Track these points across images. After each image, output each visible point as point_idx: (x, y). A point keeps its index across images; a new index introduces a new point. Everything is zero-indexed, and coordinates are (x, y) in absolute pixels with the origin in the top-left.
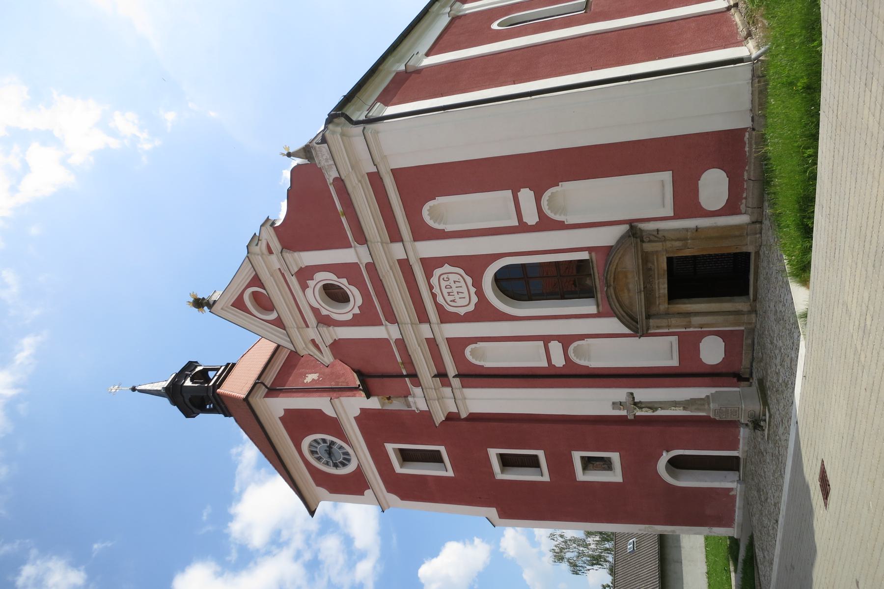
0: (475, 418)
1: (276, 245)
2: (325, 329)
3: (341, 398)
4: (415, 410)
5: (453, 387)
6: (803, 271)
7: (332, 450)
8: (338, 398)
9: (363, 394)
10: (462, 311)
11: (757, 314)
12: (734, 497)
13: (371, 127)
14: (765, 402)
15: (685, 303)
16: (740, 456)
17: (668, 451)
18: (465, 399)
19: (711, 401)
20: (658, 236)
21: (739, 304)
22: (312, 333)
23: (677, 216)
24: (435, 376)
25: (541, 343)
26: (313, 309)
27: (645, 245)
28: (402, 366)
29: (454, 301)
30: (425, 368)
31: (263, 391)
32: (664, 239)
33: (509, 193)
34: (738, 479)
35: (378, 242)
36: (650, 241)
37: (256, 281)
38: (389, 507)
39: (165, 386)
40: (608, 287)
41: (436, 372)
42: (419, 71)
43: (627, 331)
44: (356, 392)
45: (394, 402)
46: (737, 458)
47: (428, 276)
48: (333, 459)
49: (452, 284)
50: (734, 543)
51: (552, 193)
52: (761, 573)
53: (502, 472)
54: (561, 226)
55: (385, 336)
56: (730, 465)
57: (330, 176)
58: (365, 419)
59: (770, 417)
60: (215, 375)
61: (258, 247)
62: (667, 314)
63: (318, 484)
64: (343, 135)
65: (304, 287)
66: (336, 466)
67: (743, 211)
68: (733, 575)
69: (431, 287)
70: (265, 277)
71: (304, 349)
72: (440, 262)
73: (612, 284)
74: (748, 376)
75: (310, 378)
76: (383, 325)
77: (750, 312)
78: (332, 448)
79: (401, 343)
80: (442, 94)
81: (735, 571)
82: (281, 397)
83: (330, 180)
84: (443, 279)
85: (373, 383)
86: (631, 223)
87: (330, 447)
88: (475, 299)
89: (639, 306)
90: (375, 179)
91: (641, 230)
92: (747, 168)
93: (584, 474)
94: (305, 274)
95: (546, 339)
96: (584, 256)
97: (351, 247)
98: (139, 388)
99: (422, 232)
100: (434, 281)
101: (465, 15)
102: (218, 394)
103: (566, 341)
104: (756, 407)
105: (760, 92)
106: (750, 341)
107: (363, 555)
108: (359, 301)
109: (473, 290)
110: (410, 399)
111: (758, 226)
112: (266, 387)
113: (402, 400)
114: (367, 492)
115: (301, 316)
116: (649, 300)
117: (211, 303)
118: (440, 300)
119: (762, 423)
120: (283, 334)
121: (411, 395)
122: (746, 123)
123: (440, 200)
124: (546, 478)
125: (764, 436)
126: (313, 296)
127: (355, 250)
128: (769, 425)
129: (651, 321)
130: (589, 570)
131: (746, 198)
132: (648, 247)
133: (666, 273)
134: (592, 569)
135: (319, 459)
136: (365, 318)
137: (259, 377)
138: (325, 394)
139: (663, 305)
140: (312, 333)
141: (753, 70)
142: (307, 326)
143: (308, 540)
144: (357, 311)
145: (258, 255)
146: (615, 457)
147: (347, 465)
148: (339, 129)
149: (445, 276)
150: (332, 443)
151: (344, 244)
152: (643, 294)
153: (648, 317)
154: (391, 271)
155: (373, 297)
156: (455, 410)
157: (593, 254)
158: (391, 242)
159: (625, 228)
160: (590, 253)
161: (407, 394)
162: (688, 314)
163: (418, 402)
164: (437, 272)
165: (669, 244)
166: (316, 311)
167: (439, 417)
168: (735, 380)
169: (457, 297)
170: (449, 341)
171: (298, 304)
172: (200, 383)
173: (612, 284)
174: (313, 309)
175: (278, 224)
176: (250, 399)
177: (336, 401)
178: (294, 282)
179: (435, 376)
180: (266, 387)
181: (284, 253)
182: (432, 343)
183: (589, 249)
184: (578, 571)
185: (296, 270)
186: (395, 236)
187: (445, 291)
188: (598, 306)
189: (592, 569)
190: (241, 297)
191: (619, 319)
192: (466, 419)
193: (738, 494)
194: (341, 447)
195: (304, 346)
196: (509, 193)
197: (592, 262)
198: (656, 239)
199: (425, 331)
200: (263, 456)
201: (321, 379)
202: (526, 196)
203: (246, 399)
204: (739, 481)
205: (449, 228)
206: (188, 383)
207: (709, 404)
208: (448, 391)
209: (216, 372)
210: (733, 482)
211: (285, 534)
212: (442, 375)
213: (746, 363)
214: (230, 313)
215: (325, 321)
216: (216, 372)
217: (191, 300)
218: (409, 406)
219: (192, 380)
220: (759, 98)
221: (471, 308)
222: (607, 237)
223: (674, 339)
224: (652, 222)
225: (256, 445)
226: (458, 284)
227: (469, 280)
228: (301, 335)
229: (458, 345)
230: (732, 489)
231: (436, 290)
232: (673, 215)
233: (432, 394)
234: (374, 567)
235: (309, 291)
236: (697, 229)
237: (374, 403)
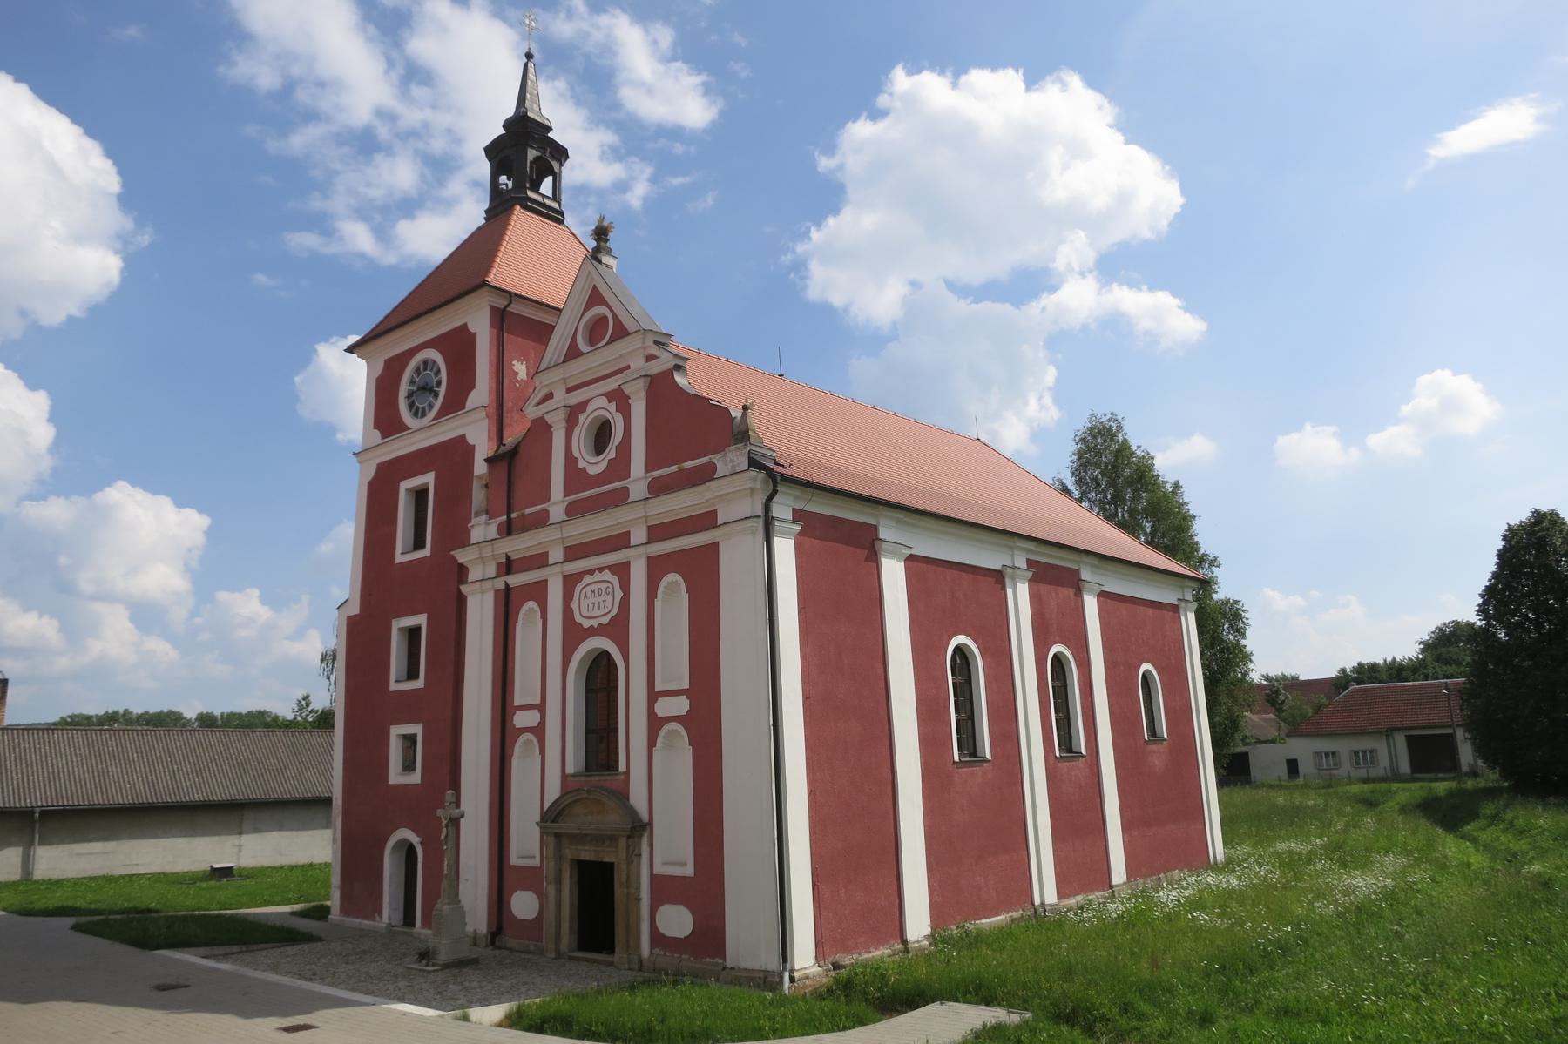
0: (461, 601)
1: (655, 368)
2: (563, 416)
3: (487, 420)
4: (471, 522)
5: (495, 580)
6: (515, 1021)
7: (427, 393)
8: (487, 416)
9: (491, 454)
10: (574, 605)
11: (555, 959)
12: (373, 919)
13: (760, 524)
14: (446, 966)
15: (571, 878)
16: (415, 930)
17: (421, 843)
18: (482, 593)
19: (451, 906)
20: (633, 855)
21: (567, 939)
22: (560, 397)
23: (654, 879)
24: (508, 557)
25: (539, 702)
26: (586, 402)
27: (625, 839)
28: (520, 513)
29: (586, 596)
30: (518, 545)
31: (501, 303)
32: (629, 862)
33: (686, 685)
34: (393, 924)
35: (646, 512)
36: (628, 846)
37: (621, 332)
38: (360, 463)
39: (529, 114)
40: (588, 791)
41: (513, 558)
42: (873, 557)
43: (546, 806)
44: (495, 440)
45: (483, 492)
46: (413, 925)
47: (614, 569)
48: (418, 393)
49: (602, 598)
50: (321, 913)
51: (683, 736)
52: (271, 951)
53: (401, 629)
54: (652, 742)
55: (553, 498)
56: (409, 919)
57: (718, 460)
58: (459, 450)
59: (429, 972)
60: (543, 196)
61: (652, 344)
62: (559, 857)
63: (389, 363)
64: (752, 490)
65: (610, 396)
66: (410, 395)
67: (654, 951)
68: (286, 908)
69: (601, 570)
70: (622, 346)
71: (541, 383)
72: (625, 586)
73: (591, 797)
74: (497, 943)
75: (521, 369)
76: (566, 496)
77: (557, 951)
78: (430, 394)
79: (541, 520)
80: (804, 608)
81: (293, 914)
82: (490, 332)
83: (715, 458)
84: (608, 587)
85: (504, 466)
86: (650, 824)
87: (431, 390)
88: (586, 624)
89: (568, 826)
90: (707, 520)
91: (640, 837)
92: (692, 959)
93: (399, 735)
94: (620, 399)
95: (541, 707)
96: (622, 767)
97: (647, 471)
98: (531, 65)
99: (657, 568)
100: (607, 575)
101: (1004, 589)
102: (511, 208)
103: (539, 731)
104: (443, 957)
105: (751, 979)
106: (532, 948)
107: (382, 233)
108: (592, 470)
109: (595, 623)
110: (484, 518)
111: (636, 967)
112: (507, 306)
113: (484, 505)
114: (377, 433)
115: (578, 385)
116: (579, 838)
117: (599, 256)
118: (588, 579)
119: (424, 962)
120: (557, 360)
121: (490, 519)
122: (729, 964)
123: (685, 597)
124: (394, 687)
125: (410, 964)
126: (601, 407)
127: (642, 478)
128: (420, 970)
129: (553, 838)
130: (329, 678)
131: (665, 955)
132: (622, 843)
133: (599, 860)
134: (330, 684)
135: (417, 371)
136: (576, 477)
137: (517, 295)
138: (494, 396)
139: (570, 852)
140: (560, 397)
141: (774, 972)
142: (569, 391)
143: (411, 134)
144: (581, 464)
145: (644, 343)
146: (415, 778)
147: (411, 411)
148: (758, 485)
149: (611, 590)
150: (436, 395)
151: (650, 466)
152: (578, 832)
153: (558, 836)
154: (615, 522)
155: (593, 491)
156: (471, 577)
157: (622, 777)
158: (649, 527)
159: (645, 817)
160: (624, 773)
161: (490, 513)
162: (558, 881)
163: (482, 529)
164: (615, 580)
165: (624, 866)
166: (582, 406)
167: (462, 556)
168: (494, 929)
169: (589, 601)
170: (543, 584)
171: (585, 386)
172: (531, 175)
173: (591, 797)
174: (586, 402)
175: (680, 379)
176: (486, 289)
177: (483, 414)
178: (611, 385)
179: (508, 557)
180: (507, 306)
181: (642, 380)
182: (540, 560)
183: (627, 773)
184: (326, 662)
185: (627, 391)
186: (657, 533)
187: (595, 587)
188: (573, 776)
189: (330, 684)
190: (604, 302)
191: (557, 800)
192: (459, 591)
193: (376, 924)
194: (431, 406)
195: (544, 384)
196: (686, 685)
197: (616, 775)
198: (630, 852)
199: (556, 555)
200: (428, 272)
201: (518, 385)
202: (681, 705)
203: (485, 284)
204: (390, 925)
205: (658, 604)
206: (532, 154)
207: (449, 904)
208: (491, 570)
209: (551, 196)
210: (389, 918)
211: (417, 91)
212: (508, 566)
213: (512, 942)
214: (586, 282)
215: (573, 413)
216: (551, 196)
217: (605, 223)
218: (477, 515)
219: (537, 159)
220: (746, 977)
221: (578, 619)
222: (638, 798)
223: (536, 862)
224: (649, 849)
225: (453, 253)
226: (602, 604)
227: (605, 620)
228: (556, 381)
229: (538, 592)
230: (381, 917)
231: (598, 576)
232: (655, 873)
233: (487, 552)
234: (362, 256)
235: (603, 402)
236: (638, 900)
237: (480, 468)
